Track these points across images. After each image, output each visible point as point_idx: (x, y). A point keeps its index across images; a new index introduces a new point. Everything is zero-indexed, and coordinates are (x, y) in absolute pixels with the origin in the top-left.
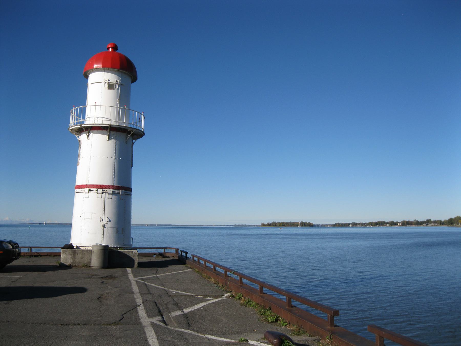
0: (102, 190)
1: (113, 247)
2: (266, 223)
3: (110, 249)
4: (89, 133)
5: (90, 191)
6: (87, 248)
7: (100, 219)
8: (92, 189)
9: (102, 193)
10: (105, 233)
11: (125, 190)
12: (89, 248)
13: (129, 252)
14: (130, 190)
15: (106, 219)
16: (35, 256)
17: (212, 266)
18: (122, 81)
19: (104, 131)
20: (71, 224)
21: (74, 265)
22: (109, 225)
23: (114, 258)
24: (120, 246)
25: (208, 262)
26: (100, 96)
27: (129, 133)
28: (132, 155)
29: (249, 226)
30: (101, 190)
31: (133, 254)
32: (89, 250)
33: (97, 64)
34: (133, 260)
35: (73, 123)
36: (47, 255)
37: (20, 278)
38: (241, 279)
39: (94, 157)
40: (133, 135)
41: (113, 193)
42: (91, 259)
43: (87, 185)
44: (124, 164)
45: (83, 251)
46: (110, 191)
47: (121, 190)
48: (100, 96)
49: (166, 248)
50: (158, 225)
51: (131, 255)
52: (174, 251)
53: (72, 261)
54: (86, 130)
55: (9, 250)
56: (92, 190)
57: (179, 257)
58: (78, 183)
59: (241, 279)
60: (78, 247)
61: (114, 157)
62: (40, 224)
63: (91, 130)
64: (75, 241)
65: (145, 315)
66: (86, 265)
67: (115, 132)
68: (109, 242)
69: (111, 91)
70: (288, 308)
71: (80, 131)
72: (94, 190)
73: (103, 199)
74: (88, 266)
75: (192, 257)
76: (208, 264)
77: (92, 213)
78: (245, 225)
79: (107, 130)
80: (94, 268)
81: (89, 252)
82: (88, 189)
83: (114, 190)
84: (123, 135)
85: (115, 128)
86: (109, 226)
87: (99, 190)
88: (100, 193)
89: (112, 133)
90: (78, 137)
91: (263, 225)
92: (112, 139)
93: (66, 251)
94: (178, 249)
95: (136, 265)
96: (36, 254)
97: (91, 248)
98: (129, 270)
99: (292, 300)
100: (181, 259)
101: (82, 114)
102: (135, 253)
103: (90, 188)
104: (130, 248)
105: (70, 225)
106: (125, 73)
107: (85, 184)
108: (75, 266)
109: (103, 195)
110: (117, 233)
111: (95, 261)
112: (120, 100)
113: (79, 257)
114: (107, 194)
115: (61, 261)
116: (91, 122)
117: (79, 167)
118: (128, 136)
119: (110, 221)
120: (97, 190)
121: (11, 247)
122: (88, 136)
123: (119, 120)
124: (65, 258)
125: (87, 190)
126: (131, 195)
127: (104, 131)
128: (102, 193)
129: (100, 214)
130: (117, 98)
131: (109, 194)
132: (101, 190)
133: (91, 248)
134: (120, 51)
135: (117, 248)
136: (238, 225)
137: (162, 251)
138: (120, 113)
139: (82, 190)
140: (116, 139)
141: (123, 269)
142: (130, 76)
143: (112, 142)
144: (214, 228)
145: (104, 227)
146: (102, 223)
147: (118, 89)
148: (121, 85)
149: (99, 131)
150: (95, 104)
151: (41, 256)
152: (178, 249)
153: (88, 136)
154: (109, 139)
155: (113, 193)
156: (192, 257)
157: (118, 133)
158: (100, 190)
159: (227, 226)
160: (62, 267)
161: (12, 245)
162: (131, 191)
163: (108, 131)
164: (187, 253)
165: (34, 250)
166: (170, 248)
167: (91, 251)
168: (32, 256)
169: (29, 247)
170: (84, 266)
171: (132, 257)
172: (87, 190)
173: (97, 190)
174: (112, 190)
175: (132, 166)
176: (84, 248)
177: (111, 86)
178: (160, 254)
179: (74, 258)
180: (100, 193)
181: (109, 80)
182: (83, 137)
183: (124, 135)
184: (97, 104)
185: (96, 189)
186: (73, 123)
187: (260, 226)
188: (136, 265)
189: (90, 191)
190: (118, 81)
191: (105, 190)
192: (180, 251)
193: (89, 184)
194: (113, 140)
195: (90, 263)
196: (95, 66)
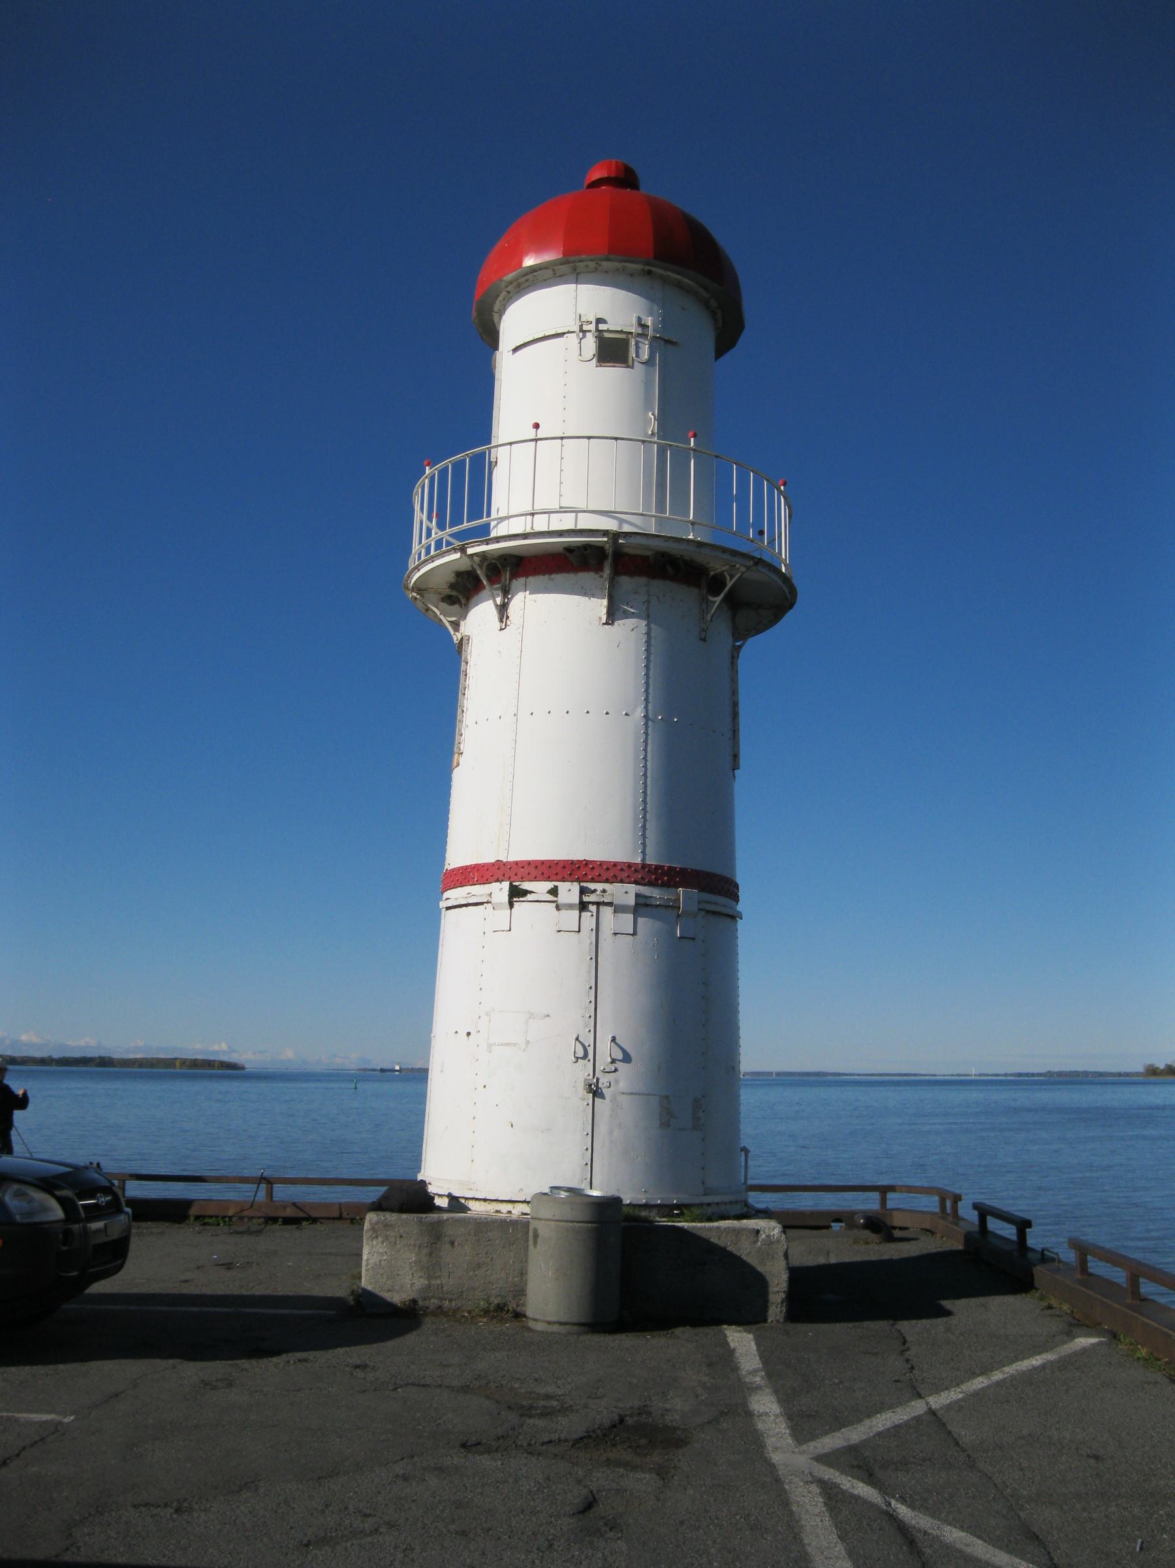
0: (583, 891)
1: (646, 1206)
2: (1162, 1066)
3: (629, 1218)
4: (506, 592)
5: (516, 893)
6: (505, 1208)
7: (569, 1048)
8: (526, 886)
9: (583, 906)
10: (602, 1129)
11: (702, 890)
12: (517, 1210)
13: (738, 1232)
14: (727, 888)
15: (605, 1050)
16: (288, 1221)
17: (1119, 1276)
18: (665, 321)
19: (581, 575)
20: (426, 1071)
21: (434, 1302)
22: (623, 1081)
23: (646, 1266)
24: (684, 1198)
25: (1094, 1255)
26: (562, 407)
27: (716, 583)
28: (735, 705)
29: (1101, 1074)
30: (575, 887)
31: (763, 1244)
32: (514, 1223)
33: (539, 249)
34: (759, 1282)
35: (431, 556)
36: (340, 1218)
37: (57, 1427)
38: (1134, 1281)
39: (541, 715)
40: (734, 603)
41: (642, 906)
42: (523, 1273)
43: (499, 864)
44: (692, 753)
45: (483, 1226)
46: (626, 893)
47: (681, 887)
48: (562, 407)
49: (892, 1188)
50: (778, 1074)
51: (745, 1250)
52: (931, 1203)
53: (420, 1282)
54: (492, 582)
55: (37, 1232)
56: (525, 893)
57: (968, 1237)
58: (458, 856)
59: (1134, 1281)
60: (456, 1204)
61: (640, 713)
62: (382, 1070)
63: (515, 575)
64: (444, 1170)
65: (782, 1427)
66: (500, 1308)
67: (643, 580)
68: (617, 1177)
69: (613, 373)
70: (1129, 1301)
71: (464, 589)
72: (540, 888)
73: (587, 936)
74: (508, 1311)
75: (1069, 1256)
76: (1097, 1267)
77: (532, 1015)
78: (1086, 1074)
79: (598, 569)
80: (539, 1327)
81: (511, 1233)
82: (506, 885)
83: (645, 890)
84: (685, 597)
85: (645, 559)
86: (623, 1086)
87: (563, 887)
88: (570, 907)
89: (626, 581)
90: (456, 625)
91: (1152, 1071)
92: (627, 615)
93: (387, 1226)
94: (957, 1198)
95: (776, 1310)
96: (290, 1212)
97: (526, 1209)
98: (742, 1342)
99: (1141, 1280)
100: (993, 1262)
101: (471, 492)
102: (770, 1242)
103: (516, 877)
104: (738, 1209)
105: (420, 1075)
106: (679, 285)
107: (490, 859)
108: (440, 1311)
109: (588, 919)
110: (664, 1124)
111: (549, 1290)
112: (662, 419)
113: (458, 1256)
114: (607, 912)
115: (365, 1283)
116: (517, 526)
117: (458, 776)
118: (709, 604)
119: (627, 1058)
120: (554, 892)
121: (58, 1213)
122: (503, 609)
123: (661, 506)
124: (383, 1262)
125: (500, 891)
126: (734, 917)
127: (587, 577)
128: (583, 906)
129: (570, 1021)
130: (648, 407)
131: (619, 909)
132: (575, 887)
133: (526, 1209)
134: (649, 187)
135: (667, 1209)
136: (1060, 1074)
137: (869, 1203)
138: (665, 481)
139: (478, 891)
140: (648, 617)
141: (707, 1333)
142: (707, 305)
143: (630, 631)
144: (1000, 1083)
145: (595, 1092)
146: (583, 1071)
147: (649, 363)
148: (664, 343)
149: (559, 577)
150: (531, 433)
151: (314, 1220)
152: (957, 1198)
153: (503, 609)
154: (612, 616)
155: (642, 906)
156: (1069, 1256)
157: (658, 586)
158: (569, 892)
159: (1020, 1075)
160: (371, 1318)
161: (62, 1201)
162: (736, 899)
163: (607, 571)
164: (1023, 1225)
165: (282, 1192)
166: (910, 1189)
167: (526, 1225)
168: (274, 1220)
169: (262, 1179)
170: (486, 1312)
171: (753, 1261)
172: (500, 891)
173: (554, 892)
174: (632, 889)
175: (735, 766)
176: (491, 1208)
177: (612, 350)
178: (877, 1225)
179: (432, 1266)
180: (570, 907)
181: (599, 321)
182: (481, 617)
183: (682, 588)
184: (541, 433)
185: (549, 885)
186: (431, 556)
187: (1137, 1074)
188: (776, 1310)
189: (516, 893)
190: (649, 321)
191: (599, 886)
192: (976, 1206)
193: (513, 857)
194: (630, 622)
195: (520, 1292)
196: (529, 261)
